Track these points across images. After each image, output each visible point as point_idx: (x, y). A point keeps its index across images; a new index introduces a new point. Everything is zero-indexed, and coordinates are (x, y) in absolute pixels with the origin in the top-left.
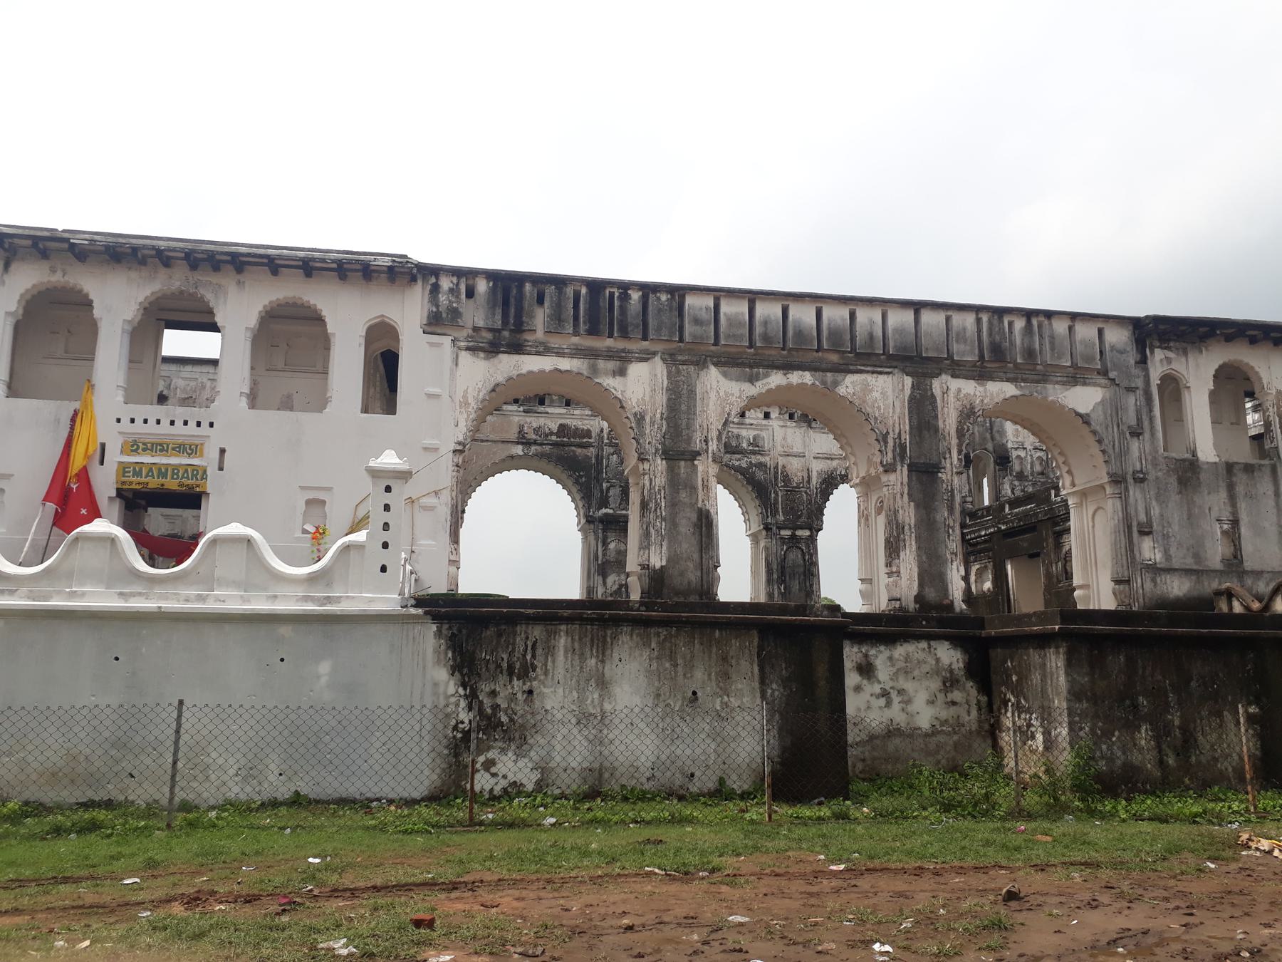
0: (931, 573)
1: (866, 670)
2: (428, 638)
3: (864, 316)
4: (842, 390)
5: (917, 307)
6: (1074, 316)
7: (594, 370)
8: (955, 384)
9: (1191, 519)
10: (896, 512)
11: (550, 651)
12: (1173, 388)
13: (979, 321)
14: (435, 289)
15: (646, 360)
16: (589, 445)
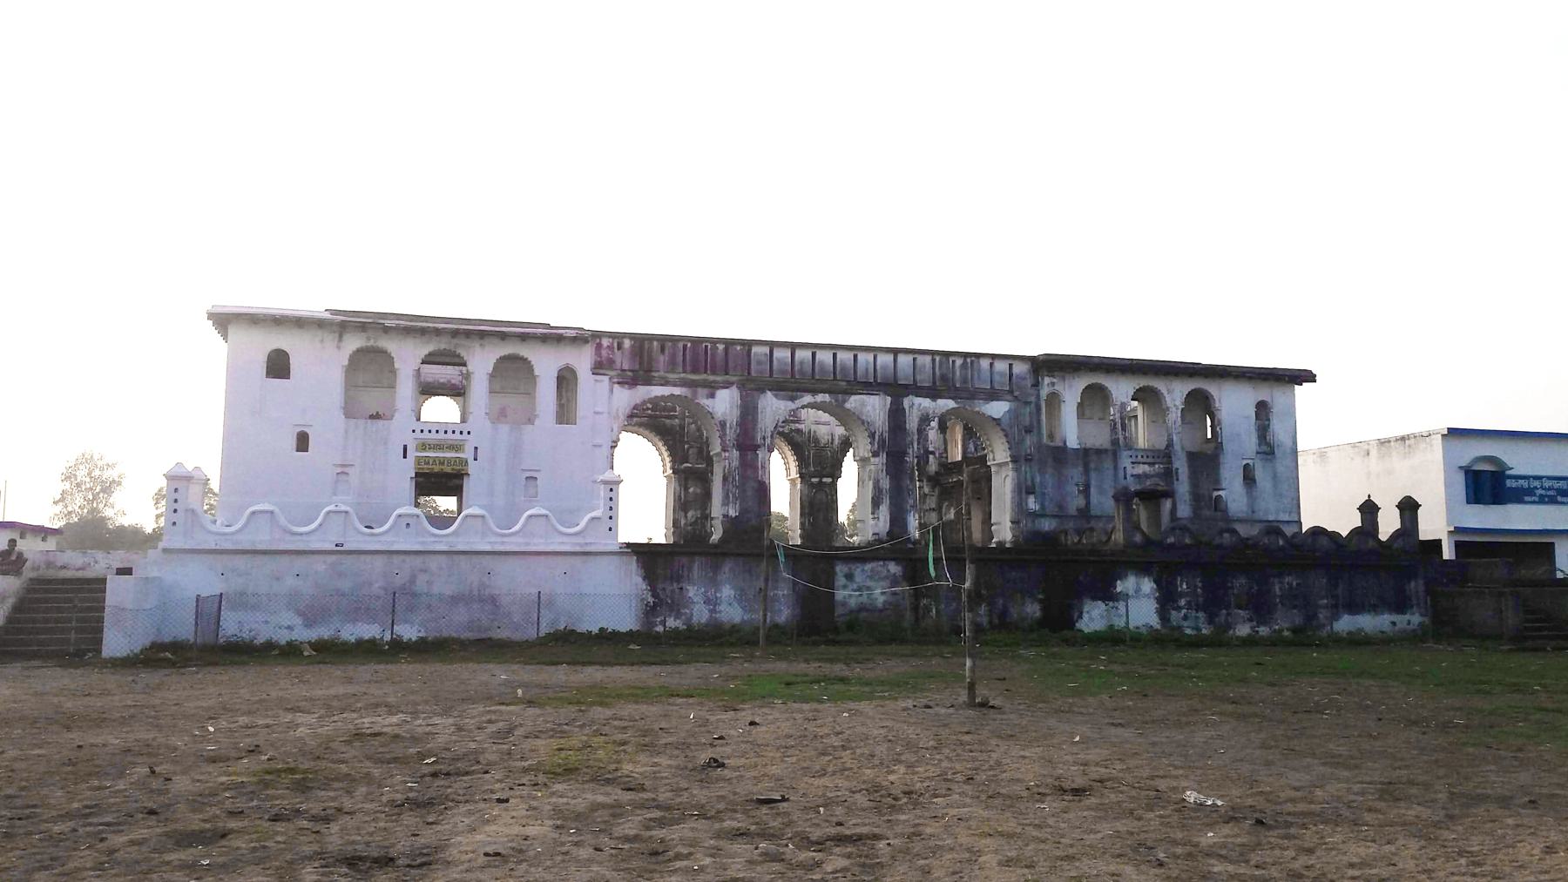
0: (898, 521)
1: (849, 577)
2: (632, 563)
3: (864, 358)
4: (848, 405)
5: (896, 352)
6: (994, 357)
7: (695, 394)
8: (918, 400)
9: (1060, 485)
10: (878, 481)
11: (690, 569)
12: (1054, 400)
13: (934, 361)
14: (599, 346)
15: (727, 388)
16: (676, 417)
